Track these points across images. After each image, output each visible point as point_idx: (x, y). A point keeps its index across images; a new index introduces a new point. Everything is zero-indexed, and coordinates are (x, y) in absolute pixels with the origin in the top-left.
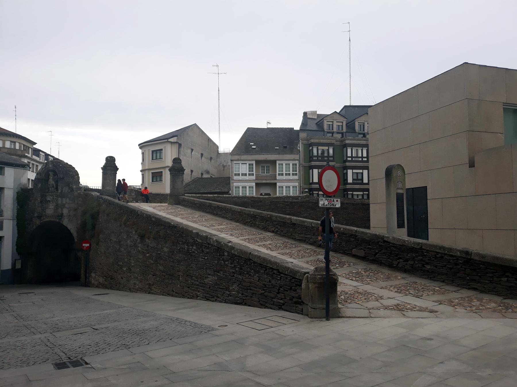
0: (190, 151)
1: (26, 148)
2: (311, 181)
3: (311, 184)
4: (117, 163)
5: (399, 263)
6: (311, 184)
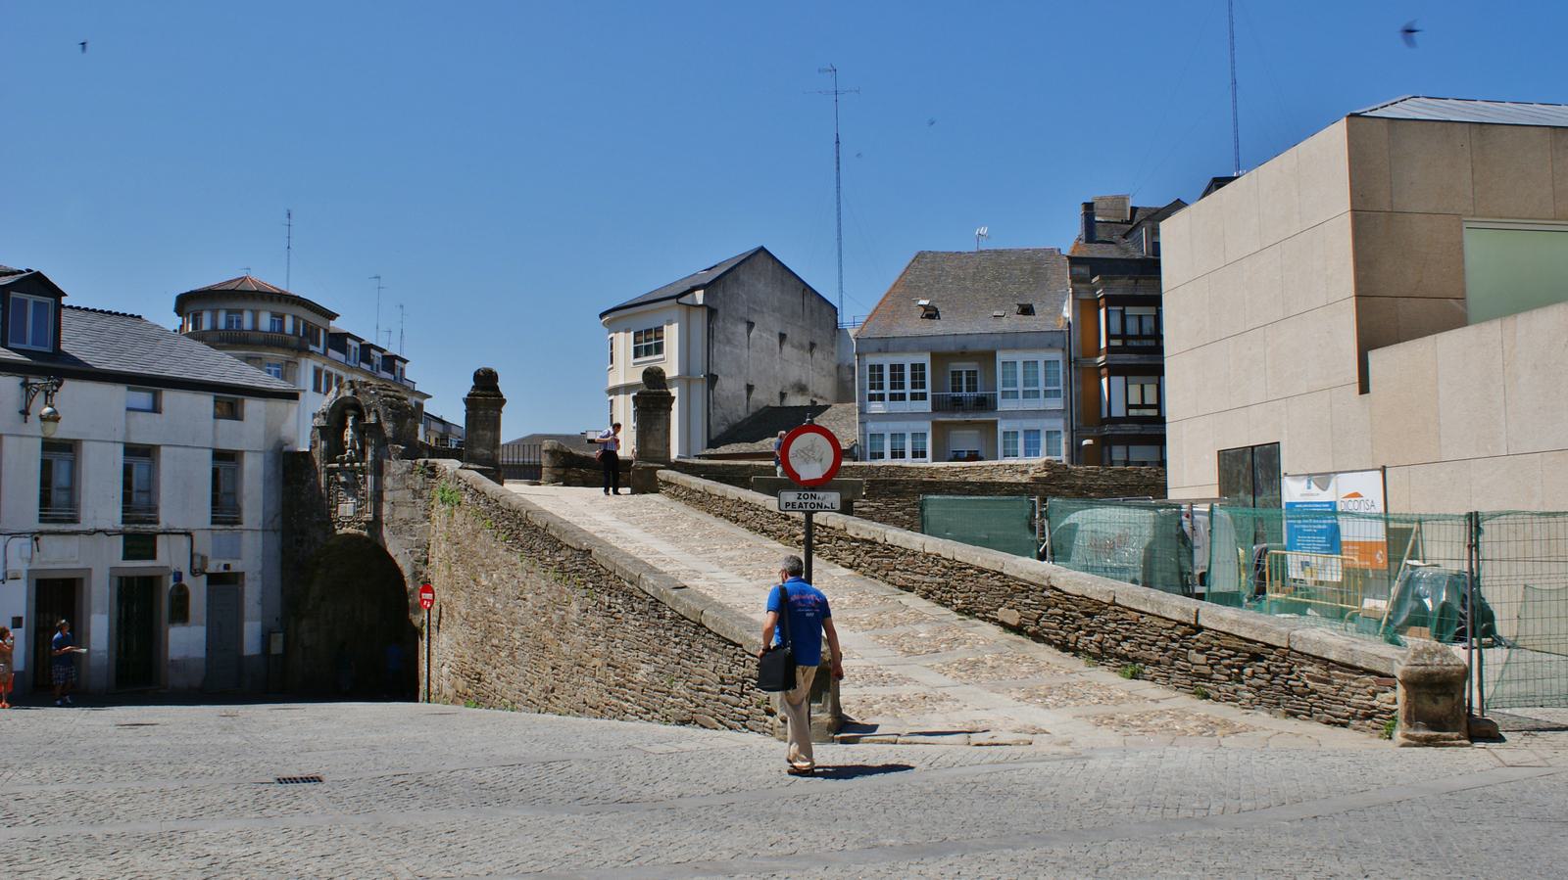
0: (742, 328)
1: (311, 334)
2: (1105, 415)
3: (1104, 422)
4: (502, 385)
5: (1078, 638)
6: (1104, 422)
